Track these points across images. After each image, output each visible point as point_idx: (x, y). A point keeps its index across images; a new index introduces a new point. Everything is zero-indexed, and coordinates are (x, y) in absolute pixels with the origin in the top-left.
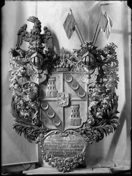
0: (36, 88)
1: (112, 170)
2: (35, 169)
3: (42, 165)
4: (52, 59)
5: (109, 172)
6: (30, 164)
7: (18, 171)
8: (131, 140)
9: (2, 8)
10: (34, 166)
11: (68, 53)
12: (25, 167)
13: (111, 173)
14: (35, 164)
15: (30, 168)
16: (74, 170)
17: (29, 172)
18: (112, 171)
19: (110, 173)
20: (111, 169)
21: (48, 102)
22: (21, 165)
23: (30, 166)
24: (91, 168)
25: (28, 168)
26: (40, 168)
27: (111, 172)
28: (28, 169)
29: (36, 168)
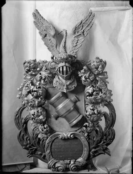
6: (25, 164)
10: (29, 167)
15: (24, 169)
25: (22, 168)
26: (34, 169)
28: (22, 169)
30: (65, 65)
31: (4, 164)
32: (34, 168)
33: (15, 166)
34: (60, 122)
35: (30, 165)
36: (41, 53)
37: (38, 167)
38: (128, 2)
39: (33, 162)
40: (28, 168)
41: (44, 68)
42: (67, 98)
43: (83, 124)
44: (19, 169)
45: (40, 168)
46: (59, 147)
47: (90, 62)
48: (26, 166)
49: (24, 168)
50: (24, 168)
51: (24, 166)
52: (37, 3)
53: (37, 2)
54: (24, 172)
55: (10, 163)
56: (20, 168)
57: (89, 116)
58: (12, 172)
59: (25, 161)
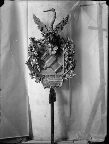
10: (25, 139)
15: (22, 141)
26: (30, 141)
28: (20, 141)
30: (53, 48)
32: (29, 140)
33: (15, 138)
34: (56, 128)
36: (39, 36)
37: (34, 140)
38: (106, 2)
39: (29, 135)
46: (36, 54)
48: (23, 139)
50: (21, 141)
51: (21, 139)
52: (29, 4)
53: (30, 3)
54: (21, 143)
56: (18, 140)
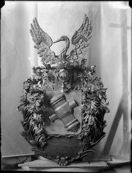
0: (29, 58)
1: (108, 164)
2: (32, 162)
3: (38, 158)
4: (41, 124)
5: (106, 166)
6: (26, 156)
7: (14, 164)
8: (1, 144)
9: (1, 9)
10: (30, 159)
11: (57, 66)
12: (22, 160)
13: (108, 167)
14: (31, 157)
15: (26, 161)
16: (71, 164)
17: (26, 167)
18: (108, 165)
19: (107, 167)
20: (107, 163)
21: (45, 68)
22: (17, 157)
23: (26, 158)
24: (87, 161)
25: (24, 160)
26: (36, 161)
27: (108, 166)
28: (24, 161)
29: (32, 161)
31: (2, 157)
35: (32, 158)
37: (40, 160)
39: (34, 154)
40: (29, 160)
41: (47, 88)
42: (66, 101)
43: (70, 163)
44: (20, 160)
45: (41, 160)
47: (96, 104)
49: (26, 160)
51: (25, 158)
55: (11, 155)
57: (85, 77)
58: (124, 85)
59: (26, 153)
